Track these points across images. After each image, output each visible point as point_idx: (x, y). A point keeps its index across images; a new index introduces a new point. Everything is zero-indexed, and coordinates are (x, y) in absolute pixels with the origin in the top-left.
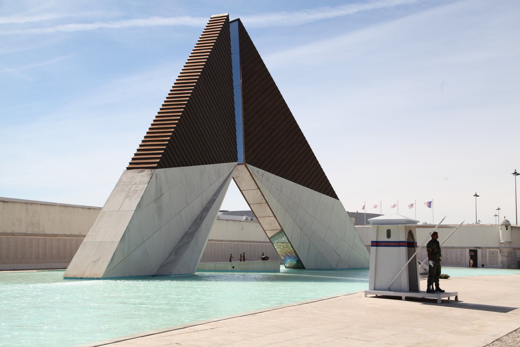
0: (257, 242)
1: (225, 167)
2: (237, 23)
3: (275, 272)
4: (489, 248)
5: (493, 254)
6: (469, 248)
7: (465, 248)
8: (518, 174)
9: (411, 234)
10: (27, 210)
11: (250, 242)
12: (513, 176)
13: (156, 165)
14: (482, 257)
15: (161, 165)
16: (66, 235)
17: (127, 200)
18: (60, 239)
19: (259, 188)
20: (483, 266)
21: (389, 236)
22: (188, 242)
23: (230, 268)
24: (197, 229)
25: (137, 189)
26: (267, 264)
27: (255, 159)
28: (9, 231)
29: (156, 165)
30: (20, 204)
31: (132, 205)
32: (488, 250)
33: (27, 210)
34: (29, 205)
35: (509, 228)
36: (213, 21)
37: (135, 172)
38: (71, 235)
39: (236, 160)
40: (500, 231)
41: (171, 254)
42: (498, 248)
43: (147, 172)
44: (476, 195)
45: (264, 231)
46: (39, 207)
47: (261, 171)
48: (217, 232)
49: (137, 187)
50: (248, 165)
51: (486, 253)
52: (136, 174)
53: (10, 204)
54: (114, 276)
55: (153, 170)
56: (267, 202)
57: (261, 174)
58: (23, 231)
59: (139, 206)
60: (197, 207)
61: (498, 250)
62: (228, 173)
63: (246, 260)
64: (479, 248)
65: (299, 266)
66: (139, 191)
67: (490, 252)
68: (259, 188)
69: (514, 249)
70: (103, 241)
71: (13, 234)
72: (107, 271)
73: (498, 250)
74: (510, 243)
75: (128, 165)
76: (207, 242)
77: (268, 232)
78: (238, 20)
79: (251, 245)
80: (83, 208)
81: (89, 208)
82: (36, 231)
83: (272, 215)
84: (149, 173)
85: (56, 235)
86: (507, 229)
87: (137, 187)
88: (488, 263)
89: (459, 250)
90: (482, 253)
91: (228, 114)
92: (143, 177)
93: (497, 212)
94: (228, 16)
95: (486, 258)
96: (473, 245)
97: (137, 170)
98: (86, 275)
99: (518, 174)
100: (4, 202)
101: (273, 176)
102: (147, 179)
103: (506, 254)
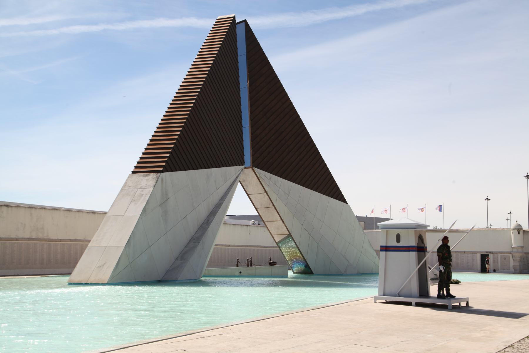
0: (265, 247)
2: (243, 24)
3: (282, 277)
4: (500, 252)
5: (505, 259)
6: (480, 252)
7: (476, 253)
9: (421, 239)
10: (31, 214)
11: (258, 247)
13: (161, 169)
15: (166, 169)
16: (70, 240)
17: (133, 204)
18: (64, 244)
19: (266, 192)
20: (494, 271)
21: (398, 240)
22: (195, 247)
23: (237, 273)
25: (142, 193)
27: (262, 162)
28: (13, 236)
29: (161, 169)
30: (24, 209)
31: (137, 209)
32: (500, 255)
33: (31, 214)
34: (33, 209)
35: (521, 232)
36: (220, 22)
37: (140, 176)
38: (75, 240)
40: (512, 235)
41: (177, 259)
42: (510, 253)
43: (153, 176)
45: (272, 235)
46: (43, 212)
48: (224, 236)
49: (142, 191)
50: (256, 169)
51: (498, 258)
52: (141, 178)
53: (13, 208)
55: (159, 174)
56: (274, 207)
58: (27, 235)
59: (144, 210)
60: (203, 211)
61: (510, 255)
62: (235, 177)
65: (307, 271)
66: (144, 196)
67: (501, 257)
68: (266, 192)
69: (526, 253)
70: (108, 246)
71: (17, 239)
72: (113, 276)
74: (522, 247)
75: (133, 169)
77: (275, 237)
79: (258, 250)
80: (88, 212)
81: (94, 213)
82: (40, 236)
83: (280, 219)
84: (155, 176)
85: (61, 240)
86: (519, 233)
88: (500, 268)
89: (470, 255)
90: (494, 258)
92: (148, 181)
93: (509, 216)
94: (234, 17)
95: (498, 263)
96: (484, 249)
97: (142, 174)
98: (92, 280)
100: (7, 206)
101: (280, 179)
103: (518, 259)
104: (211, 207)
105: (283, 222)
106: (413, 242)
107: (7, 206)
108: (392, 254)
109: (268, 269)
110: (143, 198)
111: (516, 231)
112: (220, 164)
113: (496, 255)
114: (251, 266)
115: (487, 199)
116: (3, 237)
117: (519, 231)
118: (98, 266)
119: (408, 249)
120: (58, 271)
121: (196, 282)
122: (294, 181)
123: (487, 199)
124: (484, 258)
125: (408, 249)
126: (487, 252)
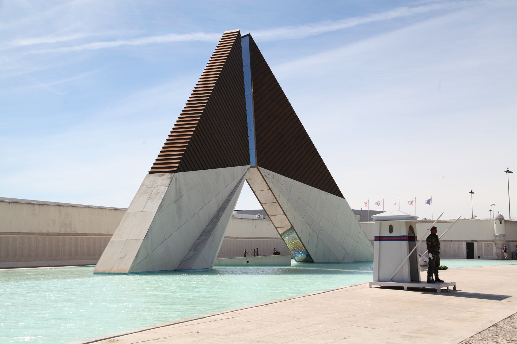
0: (269, 238)
1: (239, 170)
4: (484, 241)
5: (488, 246)
6: (466, 241)
8: (511, 172)
11: (263, 238)
12: (506, 174)
13: (175, 169)
14: (478, 249)
15: (180, 170)
16: (95, 235)
17: (150, 201)
18: (90, 238)
19: (270, 189)
21: (391, 230)
22: (206, 239)
23: (245, 263)
24: (213, 228)
26: (279, 258)
27: (266, 162)
28: (45, 231)
29: (175, 169)
30: (54, 207)
32: (483, 243)
34: (62, 207)
35: (503, 222)
38: (99, 235)
39: (248, 163)
40: (495, 225)
41: (190, 251)
43: (168, 175)
44: (508, 172)
46: (70, 209)
47: (267, 171)
49: (158, 189)
50: (260, 168)
51: (482, 245)
52: (158, 177)
53: (45, 206)
54: (139, 271)
55: (173, 174)
57: (272, 176)
58: (57, 231)
59: (161, 206)
60: (213, 207)
61: (493, 243)
62: (242, 176)
63: (256, 255)
64: (475, 241)
65: (308, 260)
67: (485, 244)
68: (270, 189)
69: (508, 241)
70: (128, 240)
71: (48, 234)
72: (133, 267)
73: (493, 243)
74: (504, 236)
75: (150, 170)
76: (223, 239)
78: (249, 35)
80: (110, 209)
82: (69, 231)
83: (282, 213)
84: (169, 176)
85: (86, 235)
87: (158, 189)
90: (478, 246)
91: (241, 119)
92: (163, 181)
93: (491, 208)
96: (470, 238)
97: (158, 174)
98: (115, 270)
99: (511, 172)
100: (39, 205)
101: (323, 192)
102: (167, 182)
103: (500, 246)
104: (221, 203)
105: (286, 216)
106: (404, 232)
107: (39, 205)
108: (383, 243)
109: (273, 258)
110: (159, 196)
111: (498, 221)
112: (228, 164)
113: (480, 243)
114: (258, 255)
115: (472, 192)
116: (36, 232)
117: (501, 221)
118: (120, 257)
119: (399, 238)
120: (75, 262)
121: (208, 271)
122: (295, 179)
123: (472, 192)
124: (470, 246)
125: (399, 238)
126: (472, 241)
